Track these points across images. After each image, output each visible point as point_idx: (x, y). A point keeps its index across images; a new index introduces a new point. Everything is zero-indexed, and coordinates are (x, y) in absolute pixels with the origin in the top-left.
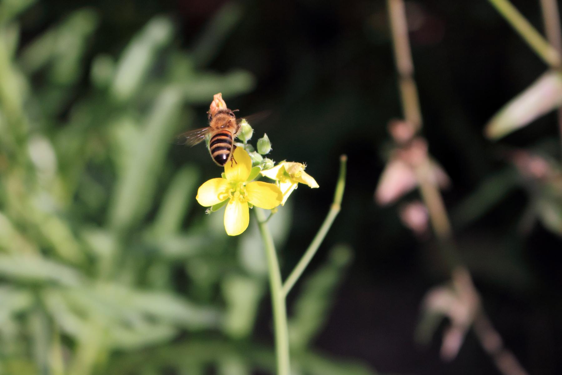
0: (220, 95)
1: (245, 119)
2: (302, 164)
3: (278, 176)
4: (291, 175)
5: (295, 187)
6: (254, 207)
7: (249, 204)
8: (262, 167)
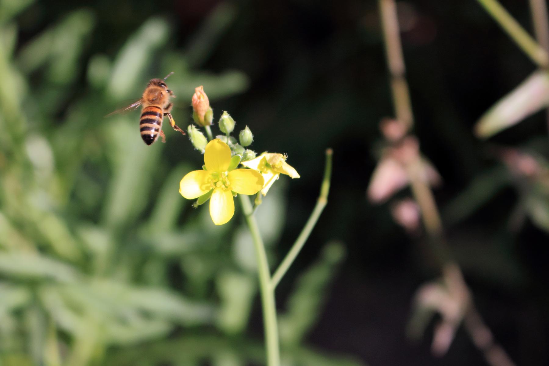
0: (202, 88)
1: (227, 111)
2: (283, 155)
3: (260, 166)
4: (272, 166)
5: (277, 177)
6: (238, 195)
7: (233, 193)
8: (241, 155)
